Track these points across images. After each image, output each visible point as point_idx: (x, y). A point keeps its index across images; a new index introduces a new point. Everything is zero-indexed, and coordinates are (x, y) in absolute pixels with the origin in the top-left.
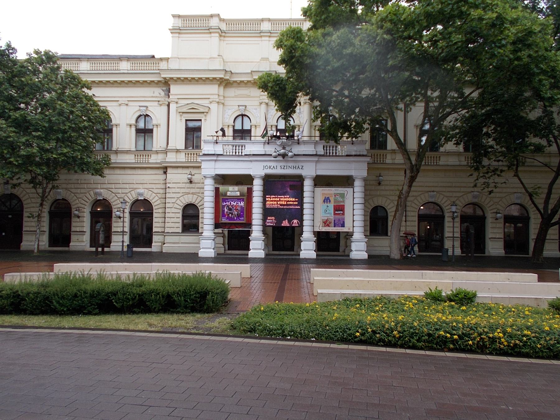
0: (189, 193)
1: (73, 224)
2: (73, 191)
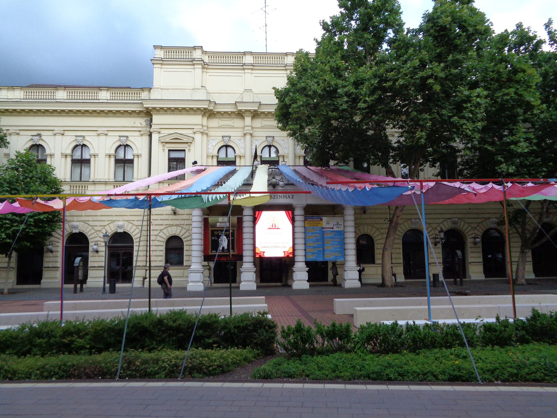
0: (173, 225)
1: (46, 259)
2: (91, 223)
